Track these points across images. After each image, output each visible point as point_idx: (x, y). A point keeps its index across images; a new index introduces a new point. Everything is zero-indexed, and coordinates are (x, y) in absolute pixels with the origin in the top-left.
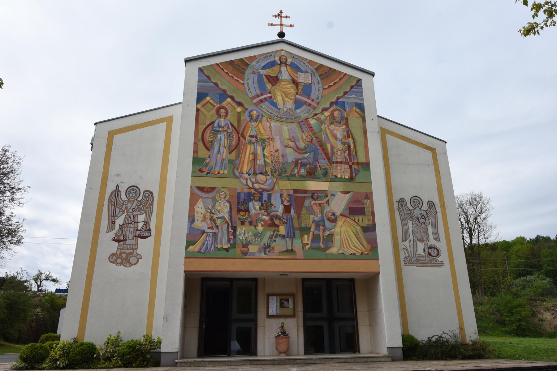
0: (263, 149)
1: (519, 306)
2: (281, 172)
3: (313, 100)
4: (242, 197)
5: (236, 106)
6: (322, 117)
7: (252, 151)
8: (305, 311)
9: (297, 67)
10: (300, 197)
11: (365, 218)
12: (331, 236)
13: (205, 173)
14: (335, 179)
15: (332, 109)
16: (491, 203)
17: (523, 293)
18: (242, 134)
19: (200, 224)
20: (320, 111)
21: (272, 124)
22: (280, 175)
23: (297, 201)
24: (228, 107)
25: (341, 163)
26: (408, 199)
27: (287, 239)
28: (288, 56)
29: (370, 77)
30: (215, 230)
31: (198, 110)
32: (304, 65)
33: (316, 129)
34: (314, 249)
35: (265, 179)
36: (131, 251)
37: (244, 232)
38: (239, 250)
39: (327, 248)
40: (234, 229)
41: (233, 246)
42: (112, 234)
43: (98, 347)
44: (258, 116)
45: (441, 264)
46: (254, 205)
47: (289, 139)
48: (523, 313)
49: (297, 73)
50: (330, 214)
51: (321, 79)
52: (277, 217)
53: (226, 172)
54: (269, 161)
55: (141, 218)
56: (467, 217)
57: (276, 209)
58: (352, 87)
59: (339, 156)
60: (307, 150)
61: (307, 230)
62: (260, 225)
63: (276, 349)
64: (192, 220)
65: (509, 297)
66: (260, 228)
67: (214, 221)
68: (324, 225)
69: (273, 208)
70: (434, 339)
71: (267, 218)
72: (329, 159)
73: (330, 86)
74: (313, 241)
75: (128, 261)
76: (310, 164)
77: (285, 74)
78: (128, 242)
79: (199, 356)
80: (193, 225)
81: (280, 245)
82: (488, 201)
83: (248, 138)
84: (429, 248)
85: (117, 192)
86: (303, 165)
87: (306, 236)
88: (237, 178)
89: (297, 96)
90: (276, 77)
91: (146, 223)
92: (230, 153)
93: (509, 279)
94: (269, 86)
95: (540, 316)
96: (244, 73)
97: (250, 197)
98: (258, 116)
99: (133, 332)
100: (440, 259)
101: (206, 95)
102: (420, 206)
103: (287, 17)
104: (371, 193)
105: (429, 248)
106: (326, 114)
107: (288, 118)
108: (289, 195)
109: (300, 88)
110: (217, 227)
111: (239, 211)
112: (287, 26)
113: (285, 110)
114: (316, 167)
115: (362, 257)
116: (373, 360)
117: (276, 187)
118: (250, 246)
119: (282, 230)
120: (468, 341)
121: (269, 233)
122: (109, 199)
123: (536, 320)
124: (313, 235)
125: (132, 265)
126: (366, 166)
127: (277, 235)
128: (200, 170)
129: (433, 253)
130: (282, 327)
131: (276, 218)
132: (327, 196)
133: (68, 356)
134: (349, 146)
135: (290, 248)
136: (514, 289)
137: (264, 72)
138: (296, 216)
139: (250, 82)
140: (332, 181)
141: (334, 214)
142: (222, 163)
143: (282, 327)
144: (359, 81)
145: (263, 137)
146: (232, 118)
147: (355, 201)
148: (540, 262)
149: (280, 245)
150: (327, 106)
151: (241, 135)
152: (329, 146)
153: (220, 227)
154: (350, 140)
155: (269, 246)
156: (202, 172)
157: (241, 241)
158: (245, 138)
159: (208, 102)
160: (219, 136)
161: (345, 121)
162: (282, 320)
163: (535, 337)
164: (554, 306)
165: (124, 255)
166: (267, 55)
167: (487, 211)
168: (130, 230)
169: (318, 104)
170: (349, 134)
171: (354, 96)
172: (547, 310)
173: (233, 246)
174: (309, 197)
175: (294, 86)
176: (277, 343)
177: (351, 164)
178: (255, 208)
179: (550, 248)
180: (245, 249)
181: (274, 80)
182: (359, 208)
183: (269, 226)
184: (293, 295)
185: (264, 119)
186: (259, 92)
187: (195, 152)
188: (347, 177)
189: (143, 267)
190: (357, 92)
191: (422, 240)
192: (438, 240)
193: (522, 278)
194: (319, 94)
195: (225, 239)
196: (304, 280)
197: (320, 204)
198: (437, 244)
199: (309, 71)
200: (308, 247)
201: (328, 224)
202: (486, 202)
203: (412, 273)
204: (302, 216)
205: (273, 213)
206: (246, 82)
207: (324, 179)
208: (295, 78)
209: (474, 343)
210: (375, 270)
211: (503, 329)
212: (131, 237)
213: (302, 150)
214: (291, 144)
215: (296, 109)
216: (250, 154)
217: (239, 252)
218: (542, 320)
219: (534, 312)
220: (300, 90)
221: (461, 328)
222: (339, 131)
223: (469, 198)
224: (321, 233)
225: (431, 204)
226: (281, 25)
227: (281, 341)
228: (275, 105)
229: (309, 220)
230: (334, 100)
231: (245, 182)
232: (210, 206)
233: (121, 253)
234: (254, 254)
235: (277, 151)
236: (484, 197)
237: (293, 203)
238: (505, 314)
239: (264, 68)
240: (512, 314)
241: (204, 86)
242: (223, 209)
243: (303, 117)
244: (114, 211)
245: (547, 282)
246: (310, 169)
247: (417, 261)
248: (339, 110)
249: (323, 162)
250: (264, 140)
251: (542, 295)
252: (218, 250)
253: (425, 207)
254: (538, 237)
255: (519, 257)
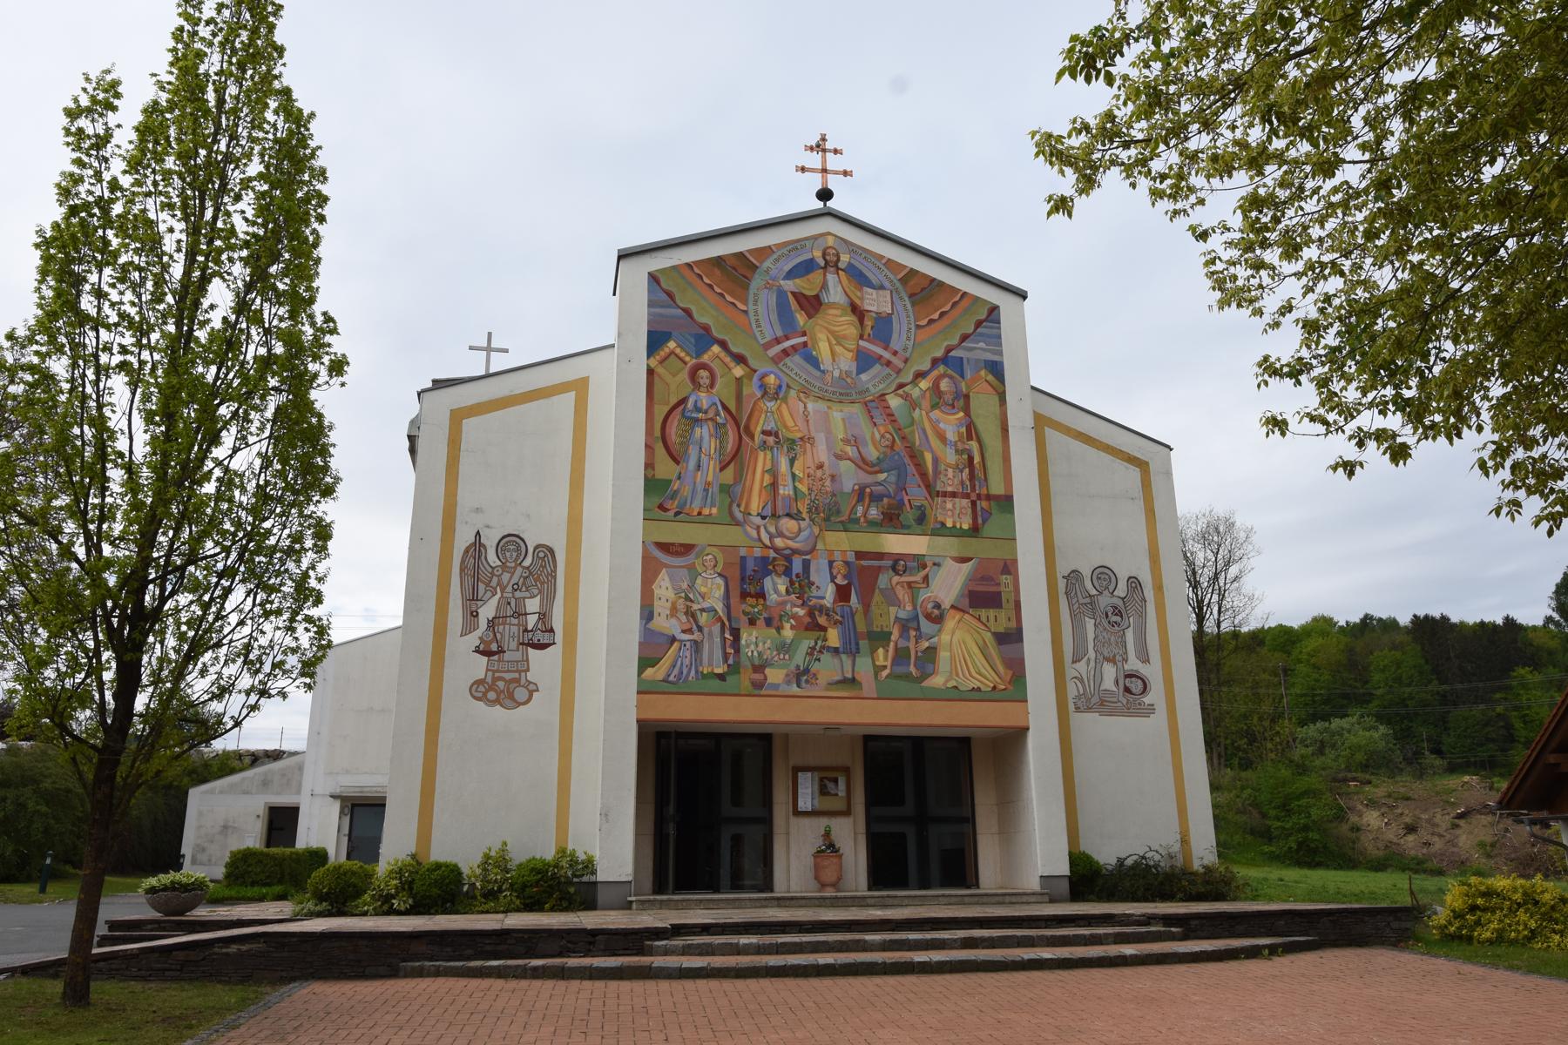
0: (792, 461)
1: (1306, 793)
2: (829, 514)
3: (895, 353)
4: (750, 565)
5: (732, 364)
6: (915, 393)
7: (768, 467)
8: (870, 803)
9: (861, 274)
10: (869, 567)
11: (1002, 615)
12: (932, 650)
13: (671, 513)
14: (941, 530)
15: (935, 373)
16: (1254, 538)
17: (1317, 763)
18: (747, 428)
19: (665, 623)
20: (910, 377)
21: (810, 406)
22: (827, 519)
23: (862, 575)
24: (715, 365)
25: (954, 495)
26: (1086, 572)
27: (844, 657)
28: (841, 248)
29: (1018, 300)
30: (696, 636)
31: (650, 372)
32: (875, 270)
33: (902, 421)
34: (899, 677)
35: (796, 529)
36: (516, 675)
37: (754, 641)
38: (745, 679)
39: (925, 676)
40: (736, 634)
41: (734, 669)
42: (473, 639)
43: (466, 871)
44: (780, 387)
45: (1149, 710)
46: (774, 584)
47: (846, 441)
48: (1315, 813)
49: (861, 290)
50: (930, 606)
51: (913, 305)
52: (821, 609)
53: (714, 511)
54: (803, 488)
55: (533, 605)
56: (1194, 573)
57: (819, 594)
58: (979, 324)
59: (950, 480)
60: (884, 466)
61: (881, 638)
62: (787, 626)
63: (816, 878)
64: (648, 614)
65: (1285, 773)
66: (788, 633)
67: (693, 616)
68: (918, 629)
69: (814, 592)
70: (1129, 862)
71: (801, 612)
72: (928, 487)
73: (931, 321)
74: (895, 662)
75: (511, 696)
76: (889, 496)
77: (836, 292)
78: (507, 656)
79: (655, 892)
80: (652, 625)
81: (828, 668)
82: (1249, 532)
83: (758, 437)
84: (1127, 676)
85: (477, 546)
86: (876, 498)
87: (881, 651)
88: (738, 524)
89: (862, 343)
90: (817, 297)
91: (544, 616)
92: (722, 469)
93: (1286, 727)
94: (801, 318)
95: (1354, 819)
96: (746, 288)
97: (766, 566)
98: (780, 387)
99: (534, 844)
100: (1147, 700)
101: (667, 337)
102: (1111, 588)
103: (836, 151)
104: (1015, 561)
105: (1127, 676)
106: (924, 384)
107: (842, 393)
108: (847, 563)
109: (868, 323)
110: (700, 629)
111: (744, 595)
112: (836, 173)
113: (836, 373)
114: (901, 504)
115: (996, 695)
116: (1014, 899)
117: (820, 546)
118: (767, 671)
119: (834, 637)
120: (1196, 866)
121: (806, 644)
122: (463, 561)
123: (1345, 828)
124: (896, 649)
125: (520, 704)
126: (1006, 502)
127: (823, 647)
128: (661, 507)
129: (1133, 689)
130: (827, 834)
131: (821, 612)
132: (924, 567)
133: (411, 889)
134: (971, 459)
135: (849, 675)
136: (1298, 752)
137: (789, 285)
138: (860, 608)
139: (761, 309)
140: (934, 533)
141: (938, 606)
142: (706, 490)
143: (827, 834)
144: (994, 309)
145: (790, 436)
146: (724, 390)
147: (983, 578)
148: (1366, 682)
149: (828, 668)
150: (926, 366)
151: (745, 432)
152: (928, 457)
153: (706, 630)
154: (974, 445)
155: (807, 671)
156: (666, 510)
157: (751, 659)
158: (752, 437)
159: (672, 352)
160: (698, 430)
161: (963, 401)
162: (823, 822)
163: (1340, 868)
164: (1389, 796)
165: (501, 684)
166: (795, 246)
167: (1245, 560)
168: (510, 631)
169: (906, 361)
170: (971, 431)
171: (982, 345)
172: (1372, 804)
173: (734, 669)
174: (886, 568)
175: (853, 318)
176: (817, 868)
177: (974, 497)
178: (776, 591)
179: (1394, 647)
180: (758, 677)
181: (812, 305)
182: (989, 594)
183: (807, 629)
184: (846, 771)
185: (793, 393)
186: (779, 333)
187: (649, 465)
188: (965, 527)
189: (542, 709)
190: (989, 336)
191: (1112, 660)
192: (1146, 660)
193: (1319, 725)
194: (908, 339)
195: (718, 654)
196: (868, 739)
197: (909, 584)
198: (1143, 670)
199: (887, 284)
200: (885, 673)
201: (926, 626)
202: (1242, 535)
203: (1091, 727)
204: (873, 608)
205: (814, 601)
206: (751, 308)
207: (918, 529)
208: (858, 302)
209: (1208, 870)
210: (1021, 724)
211: (1266, 849)
212: (513, 645)
213: (873, 465)
214: (850, 450)
215: (859, 373)
216: (764, 472)
217: (747, 683)
218: (1358, 829)
219: (1341, 809)
220: (868, 330)
221: (1185, 841)
222: (951, 424)
223: (1202, 524)
224: (912, 645)
225: (1134, 583)
226: (824, 171)
227: (826, 863)
228: (814, 362)
229: (888, 616)
230: (939, 353)
231: (754, 533)
232: (685, 586)
233: (495, 679)
234: (776, 686)
235: (820, 466)
236: (1238, 524)
237: (855, 581)
238: (1273, 813)
239: (790, 275)
240: (1289, 813)
241: (661, 315)
242: (712, 591)
243: (875, 391)
244: (475, 589)
245: (1378, 736)
246: (890, 506)
247: (1102, 703)
248: (951, 377)
249: (916, 494)
250: (793, 441)
251: (1365, 767)
252: (704, 676)
253: (1122, 590)
254: (1367, 619)
255: (1315, 667)
